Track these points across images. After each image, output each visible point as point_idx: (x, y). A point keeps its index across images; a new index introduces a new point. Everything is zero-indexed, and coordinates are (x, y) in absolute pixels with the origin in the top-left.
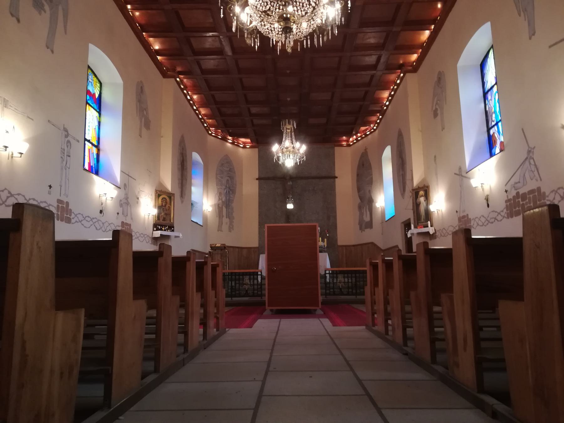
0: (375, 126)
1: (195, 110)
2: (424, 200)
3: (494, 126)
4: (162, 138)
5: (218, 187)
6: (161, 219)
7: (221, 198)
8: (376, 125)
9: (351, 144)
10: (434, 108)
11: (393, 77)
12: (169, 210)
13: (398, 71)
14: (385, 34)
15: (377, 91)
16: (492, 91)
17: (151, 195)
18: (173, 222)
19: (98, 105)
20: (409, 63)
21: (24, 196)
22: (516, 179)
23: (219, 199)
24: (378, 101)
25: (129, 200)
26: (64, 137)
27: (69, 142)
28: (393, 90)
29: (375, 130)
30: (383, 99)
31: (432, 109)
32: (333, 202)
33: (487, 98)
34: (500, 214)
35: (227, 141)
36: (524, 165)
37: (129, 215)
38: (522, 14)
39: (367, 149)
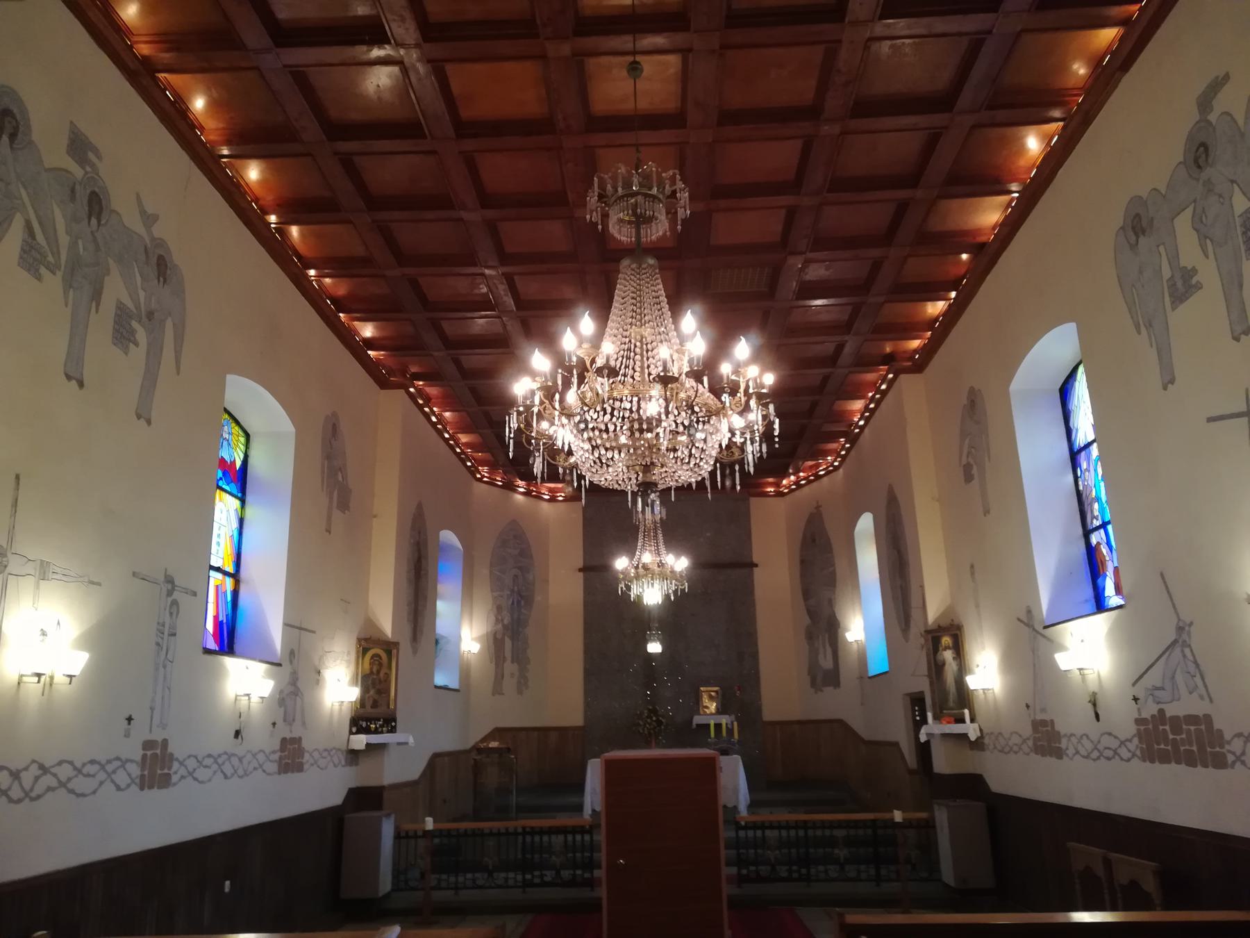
0: (835, 460)
1: (446, 440)
2: (954, 658)
3: (1097, 528)
4: (375, 519)
5: (494, 594)
6: (369, 704)
7: (500, 618)
8: (839, 459)
9: (786, 491)
10: (964, 461)
11: (871, 377)
12: (385, 681)
14: (849, 308)
15: (837, 402)
16: (1087, 450)
17: (349, 653)
20: (905, 352)
21: (71, 763)
22: (1154, 678)
24: (842, 417)
25: (299, 684)
26: (166, 593)
27: (175, 603)
28: (872, 400)
29: (836, 468)
30: (852, 413)
33: (1078, 464)
35: (515, 491)
36: (1169, 655)
37: (298, 717)
38: (1143, 329)
39: (820, 506)
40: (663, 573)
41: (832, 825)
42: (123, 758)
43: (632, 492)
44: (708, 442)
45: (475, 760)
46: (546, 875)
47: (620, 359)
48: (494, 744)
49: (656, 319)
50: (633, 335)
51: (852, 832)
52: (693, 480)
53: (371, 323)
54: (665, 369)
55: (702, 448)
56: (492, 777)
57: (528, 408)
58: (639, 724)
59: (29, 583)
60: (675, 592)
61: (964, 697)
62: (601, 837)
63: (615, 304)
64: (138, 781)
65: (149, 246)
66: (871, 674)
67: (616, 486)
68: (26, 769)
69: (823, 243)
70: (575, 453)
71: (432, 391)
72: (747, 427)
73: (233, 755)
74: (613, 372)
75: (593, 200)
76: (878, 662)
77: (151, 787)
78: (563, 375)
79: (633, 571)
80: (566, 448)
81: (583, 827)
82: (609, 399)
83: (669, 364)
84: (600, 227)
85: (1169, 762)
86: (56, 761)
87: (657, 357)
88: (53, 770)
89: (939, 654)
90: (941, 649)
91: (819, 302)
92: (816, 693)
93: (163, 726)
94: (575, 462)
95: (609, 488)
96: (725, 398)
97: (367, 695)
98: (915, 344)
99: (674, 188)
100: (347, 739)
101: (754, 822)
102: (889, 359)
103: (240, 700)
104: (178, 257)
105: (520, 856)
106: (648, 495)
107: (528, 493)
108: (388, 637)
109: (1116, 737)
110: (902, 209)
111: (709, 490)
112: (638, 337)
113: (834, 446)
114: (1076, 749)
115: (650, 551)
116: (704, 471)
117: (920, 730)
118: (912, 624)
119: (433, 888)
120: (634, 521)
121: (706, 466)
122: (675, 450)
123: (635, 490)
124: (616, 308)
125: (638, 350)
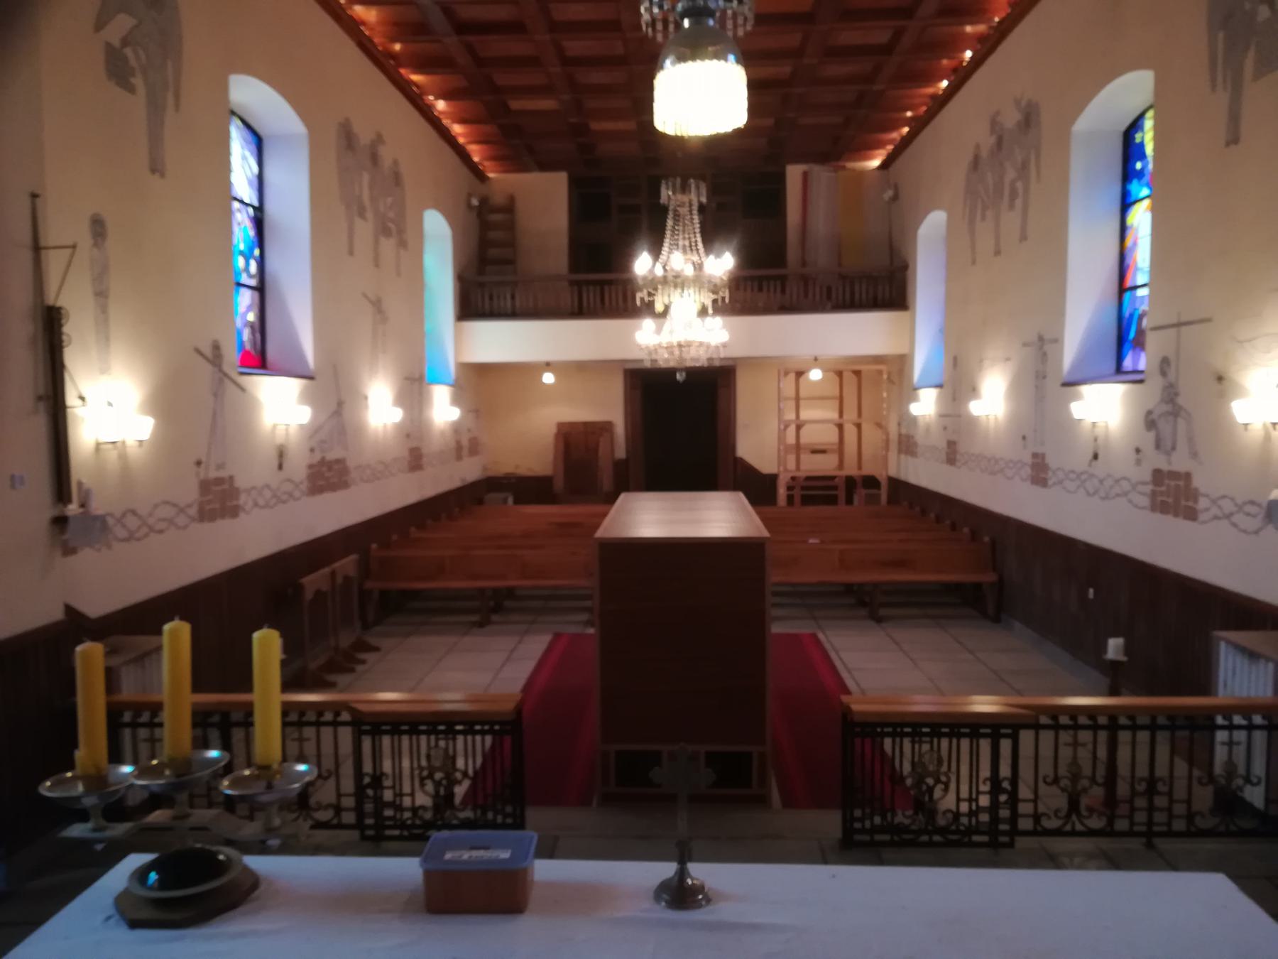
8: (918, 730)
10: (1181, 423)
25: (1180, 400)
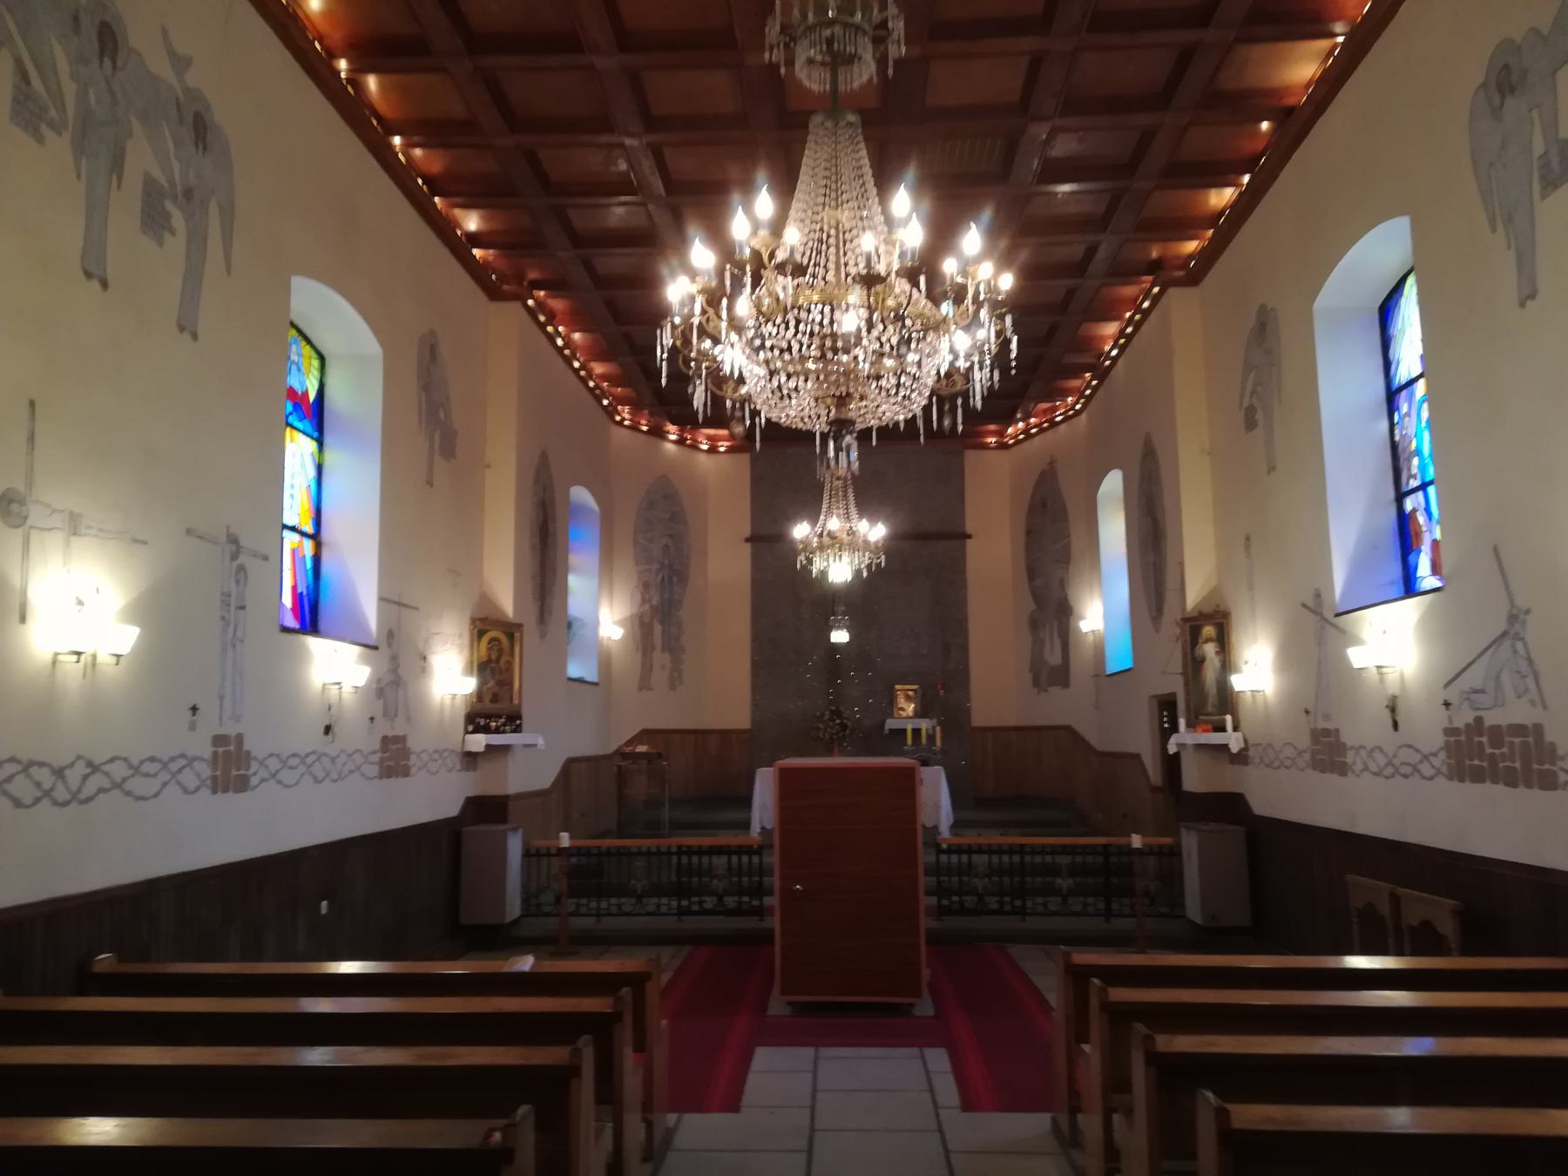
0: (1077, 403)
2: (1217, 653)
6: (487, 699)
10: (1246, 403)
11: (1129, 291)
13: (1145, 278)
16: (1410, 388)
17: (460, 636)
18: (520, 705)
19: (315, 420)
20: (1178, 257)
21: (125, 760)
22: (1474, 678)
23: (644, 601)
24: (1090, 345)
25: (400, 671)
27: (241, 568)
29: (1078, 413)
30: (1103, 339)
31: (1241, 404)
32: (962, 604)
33: (1396, 407)
34: (1428, 760)
38: (1500, 225)
40: (853, 544)
41: (1054, 851)
42: (190, 754)
43: (822, 434)
44: (922, 366)
45: (619, 767)
46: (705, 901)
47: (808, 253)
48: (642, 749)
49: (857, 198)
50: (825, 220)
51: (1079, 859)
52: (901, 417)
53: (480, 211)
54: (868, 265)
55: (915, 375)
56: (640, 788)
57: (687, 319)
58: (819, 728)
59: (55, 540)
60: (869, 567)
61: (1227, 700)
62: (773, 859)
63: (802, 177)
64: (208, 782)
65: (181, 96)
66: (1108, 672)
67: (800, 425)
68: (72, 765)
69: (1075, 105)
70: (748, 381)
71: (557, 304)
72: (974, 346)
73: (325, 755)
74: (799, 270)
75: (773, 31)
76: (1119, 657)
77: (226, 790)
78: (732, 275)
79: (816, 539)
80: (736, 375)
81: (751, 846)
82: (793, 308)
83: (874, 258)
84: (783, 70)
85: (1483, 781)
86: (109, 757)
87: (858, 251)
88: (106, 768)
89: (1197, 647)
90: (1200, 641)
91: (1066, 188)
92: (1039, 693)
93: (237, 719)
94: (747, 392)
95: (791, 428)
96: (946, 308)
97: (485, 687)
98: (1191, 246)
99: (884, 15)
100: (461, 740)
101: (959, 845)
102: (1155, 267)
103: (329, 689)
104: (222, 115)
105: (674, 879)
106: (843, 437)
107: (681, 442)
108: (508, 618)
109: (1418, 751)
110: (1186, 56)
111: (922, 432)
112: (833, 223)
113: (1076, 383)
114: (1365, 764)
115: (838, 516)
116: (915, 405)
117: (1169, 739)
118: (1166, 610)
119: (571, 914)
120: (818, 477)
121: (918, 399)
122: (878, 378)
123: (826, 431)
124: (798, 200)
125: (832, 241)
